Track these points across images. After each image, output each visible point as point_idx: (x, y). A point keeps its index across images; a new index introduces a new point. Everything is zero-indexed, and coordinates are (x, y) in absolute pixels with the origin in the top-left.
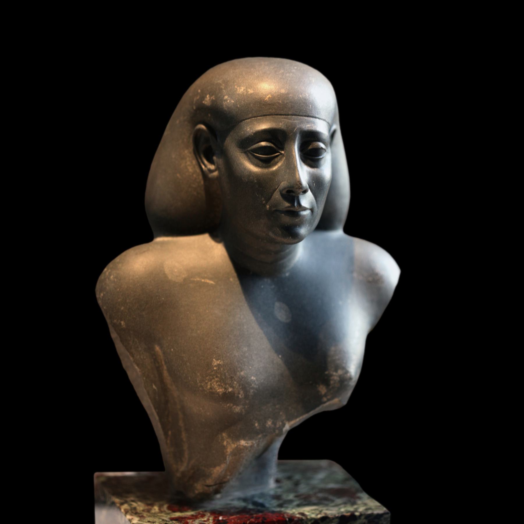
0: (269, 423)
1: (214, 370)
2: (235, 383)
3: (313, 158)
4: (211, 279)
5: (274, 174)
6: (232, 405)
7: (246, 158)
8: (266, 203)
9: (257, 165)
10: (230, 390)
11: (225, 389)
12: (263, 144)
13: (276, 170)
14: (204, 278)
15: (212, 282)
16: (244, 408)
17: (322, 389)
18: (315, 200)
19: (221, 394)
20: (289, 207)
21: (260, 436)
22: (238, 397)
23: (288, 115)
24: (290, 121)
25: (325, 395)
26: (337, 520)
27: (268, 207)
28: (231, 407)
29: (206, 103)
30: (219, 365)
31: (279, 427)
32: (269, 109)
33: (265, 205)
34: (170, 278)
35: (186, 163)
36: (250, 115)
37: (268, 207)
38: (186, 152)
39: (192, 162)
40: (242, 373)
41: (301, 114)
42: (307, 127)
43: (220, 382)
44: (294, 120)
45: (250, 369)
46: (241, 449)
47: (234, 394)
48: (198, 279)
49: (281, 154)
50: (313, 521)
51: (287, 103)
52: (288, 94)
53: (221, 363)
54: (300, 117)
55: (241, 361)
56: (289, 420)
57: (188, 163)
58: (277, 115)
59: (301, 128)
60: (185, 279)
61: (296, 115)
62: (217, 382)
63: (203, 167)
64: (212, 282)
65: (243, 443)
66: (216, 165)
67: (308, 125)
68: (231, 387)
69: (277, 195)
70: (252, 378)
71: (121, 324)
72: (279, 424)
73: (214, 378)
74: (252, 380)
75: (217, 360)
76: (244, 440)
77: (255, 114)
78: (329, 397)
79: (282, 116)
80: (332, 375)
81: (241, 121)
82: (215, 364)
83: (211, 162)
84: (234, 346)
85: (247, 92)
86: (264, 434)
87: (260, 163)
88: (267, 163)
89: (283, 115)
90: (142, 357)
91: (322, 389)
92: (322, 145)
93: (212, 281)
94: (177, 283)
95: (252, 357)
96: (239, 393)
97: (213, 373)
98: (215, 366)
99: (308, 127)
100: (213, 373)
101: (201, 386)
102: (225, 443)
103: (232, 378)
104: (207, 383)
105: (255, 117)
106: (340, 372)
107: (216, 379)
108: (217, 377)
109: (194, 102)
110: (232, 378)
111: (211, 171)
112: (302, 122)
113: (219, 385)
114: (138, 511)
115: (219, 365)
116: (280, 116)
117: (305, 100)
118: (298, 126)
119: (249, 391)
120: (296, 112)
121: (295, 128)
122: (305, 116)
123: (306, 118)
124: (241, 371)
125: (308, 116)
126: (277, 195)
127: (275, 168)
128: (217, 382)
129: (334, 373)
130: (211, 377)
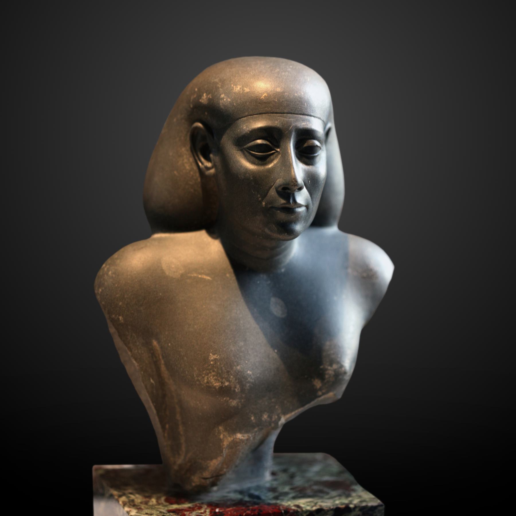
0: (265, 417)
1: (211, 364)
2: (232, 377)
3: (309, 155)
4: (207, 275)
5: (270, 171)
6: (228, 399)
7: (242, 156)
8: (262, 200)
9: (253, 163)
10: (227, 384)
11: (222, 383)
12: (259, 141)
13: (272, 168)
14: (201, 274)
15: (209, 278)
16: (241, 402)
17: (318, 383)
18: (310, 197)
19: (217, 388)
21: (256, 429)
22: (235, 391)
23: (284, 113)
24: (286, 119)
25: (320, 389)
26: (332, 512)
27: (264, 203)
28: (228, 401)
29: (203, 101)
30: (215, 360)
31: (275, 421)
32: (265, 107)
33: (260, 202)
34: (167, 274)
35: (183, 160)
36: (246, 114)
37: (264, 203)
38: (183, 149)
39: (189, 160)
40: (238, 368)
41: (296, 112)
42: (302, 125)
43: (217, 376)
44: (289, 118)
45: (247, 364)
46: (237, 442)
47: (231, 388)
48: (195, 275)
49: (277, 152)
50: (308, 513)
51: (283, 101)
52: (283, 92)
53: (218, 357)
54: (295, 115)
55: (238, 356)
56: (285, 414)
57: (186, 160)
58: (273, 113)
59: (296, 126)
60: (182, 275)
61: (291, 113)
62: (214, 376)
64: (209, 278)
65: (239, 436)
66: (213, 162)
67: (304, 124)
68: (227, 381)
69: (273, 192)
70: (249, 372)
71: (119, 319)
72: (275, 417)
73: (210, 373)
74: (248, 374)
75: (214, 354)
76: (241, 433)
77: (251, 113)
78: (324, 391)
79: (278, 115)
80: (327, 370)
81: (238, 119)
82: (212, 358)
83: (208, 159)
84: (230, 341)
85: (243, 90)
86: (260, 427)
87: (256, 161)
88: (263, 160)
89: (279, 113)
90: (140, 352)
91: (318, 383)
92: (317, 143)
93: (209, 276)
94: (174, 278)
95: (248, 352)
96: (235, 387)
97: (210, 367)
98: (212, 361)
99: (303, 125)
100: (210, 367)
101: (198, 380)
102: (222, 436)
103: (228, 372)
104: (203, 377)
105: (251, 115)
106: (335, 366)
107: (213, 373)
108: (213, 371)
109: (191, 101)
110: (228, 372)
111: (208, 169)
112: (297, 120)
113: (215, 379)
115: (215, 359)
116: (275, 114)
117: (301, 98)
118: (293, 125)
119: (246, 385)
120: (291, 110)
121: (290, 126)
122: (301, 114)
123: (301, 116)
124: (238, 365)
125: (304, 114)
126: (273, 192)
127: (270, 166)
128: (214, 376)
129: (329, 368)
130: (208, 371)
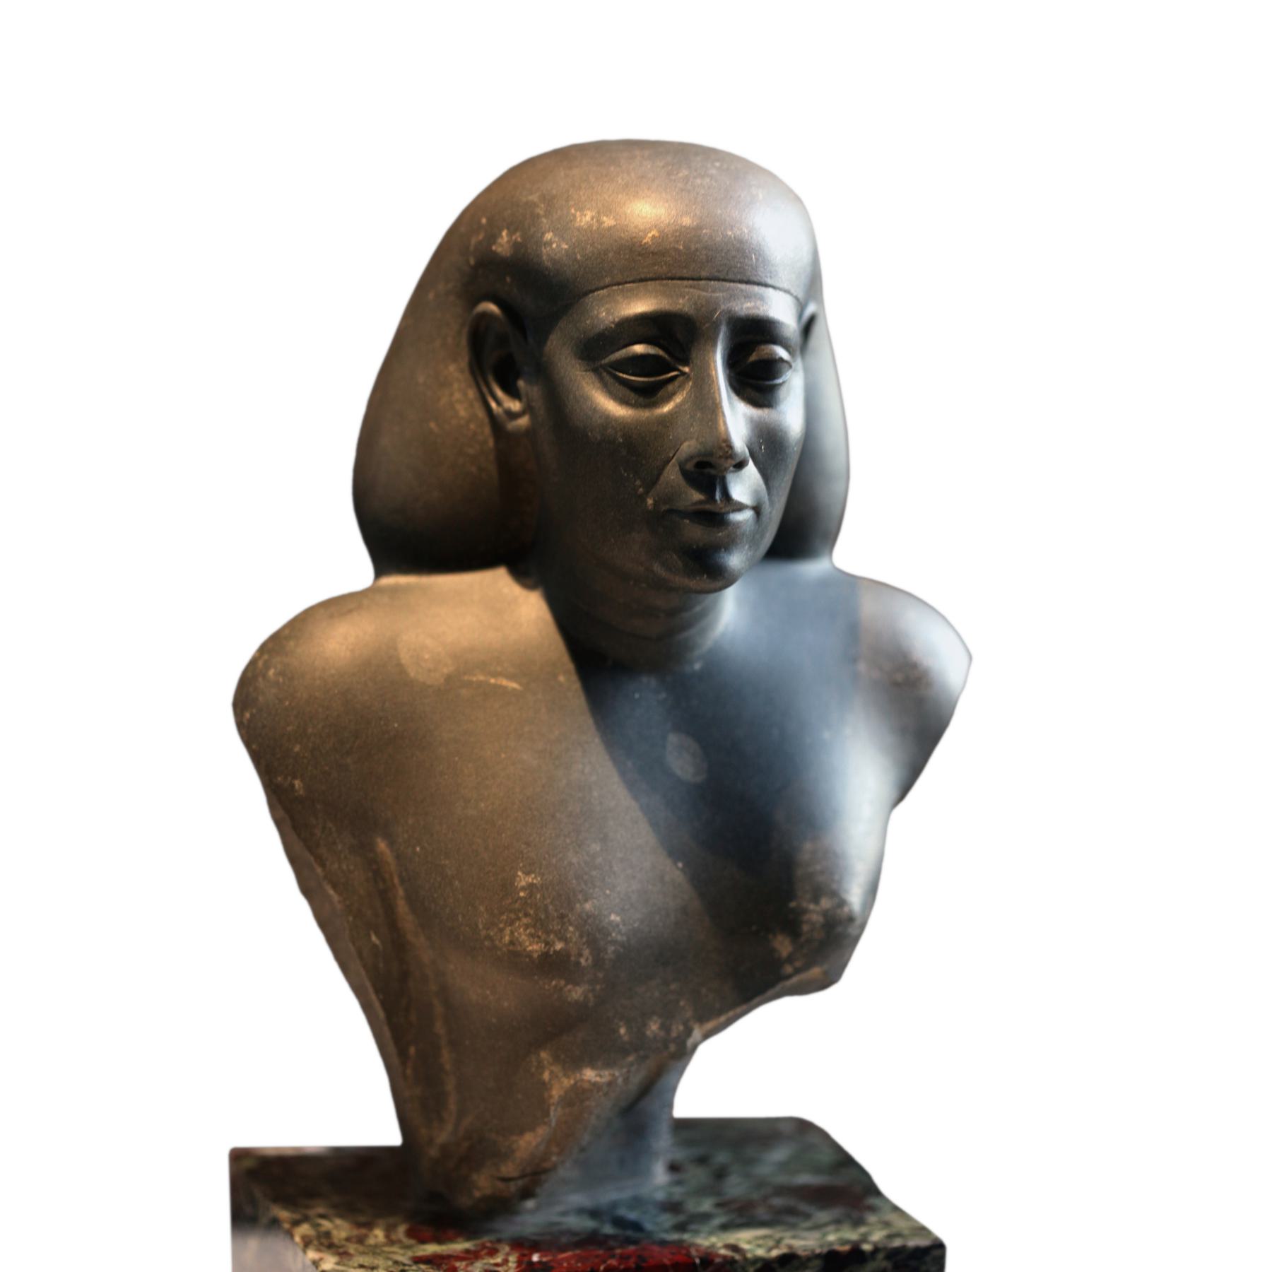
0: (654, 1027)
1: (521, 898)
2: (571, 929)
3: (761, 382)
4: (511, 677)
5: (666, 421)
6: (562, 982)
7: (598, 385)
8: (647, 493)
9: (623, 402)
10: (559, 946)
11: (547, 943)
12: (639, 349)
13: (670, 413)
14: (495, 675)
15: (514, 685)
16: (593, 990)
17: (783, 945)
18: (763, 487)
19: (535, 955)
20: (700, 502)
21: (631, 1059)
22: (578, 963)
23: (700, 279)
24: (704, 294)
25: (790, 960)
26: (817, 1263)
27: (650, 502)
28: (561, 989)
29: (499, 250)
30: (531, 886)
31: (678, 1037)
32: (654, 264)
33: (642, 498)
34: (412, 674)
35: (451, 395)
36: (608, 280)
37: (650, 502)
38: (452, 368)
39: (465, 394)
40: (588, 906)
41: (731, 276)
42: (745, 308)
43: (534, 926)
44: (713, 291)
45: (608, 896)
46: (584, 1091)
47: (569, 956)
48: (481, 678)
49: (683, 374)
50: (759, 1265)
51: (697, 250)
52: (699, 228)
53: (538, 881)
54: (728, 284)
55: (586, 877)
57: (457, 396)
58: (672, 279)
59: (730, 311)
60: (449, 678)
61: (718, 279)
62: (527, 927)
63: (493, 405)
64: (514, 685)
65: (589, 1074)
66: (524, 399)
67: (749, 305)
68: (560, 939)
69: (672, 474)
70: (613, 917)
71: (293, 786)
72: (677, 1029)
73: (519, 919)
74: (611, 923)
75: (527, 873)
76: (593, 1067)
77: (619, 278)
78: (798, 964)
79: (685, 282)
80: (805, 911)
81: (586, 294)
82: (523, 883)
83: (513, 393)
84: (568, 841)
85: (600, 223)
86: (642, 1053)
87: (632, 396)
88: (648, 395)
89: (688, 279)
90: (344, 867)
91: (783, 945)
93: (516, 681)
94: (430, 686)
95: (611, 867)
96: (580, 955)
97: (517, 905)
98: (523, 889)
99: (748, 308)
100: (517, 905)
101: (488, 937)
102: (546, 1076)
103: (562, 917)
104: (501, 930)
105: (618, 284)
106: (825, 903)
107: (525, 921)
108: (526, 915)
109: (472, 248)
110: (562, 917)
111: (512, 415)
112: (732, 297)
113: (531, 935)
114: (336, 1241)
115: (531, 885)
116: (679, 282)
117: (741, 242)
118: (723, 307)
119: (606, 950)
120: (718, 271)
121: (715, 310)
122: (741, 282)
123: (743, 286)
124: (586, 901)
125: (748, 282)
126: (672, 474)
127: (666, 409)
128: (527, 927)
129: (812, 907)
130: (513, 916)
